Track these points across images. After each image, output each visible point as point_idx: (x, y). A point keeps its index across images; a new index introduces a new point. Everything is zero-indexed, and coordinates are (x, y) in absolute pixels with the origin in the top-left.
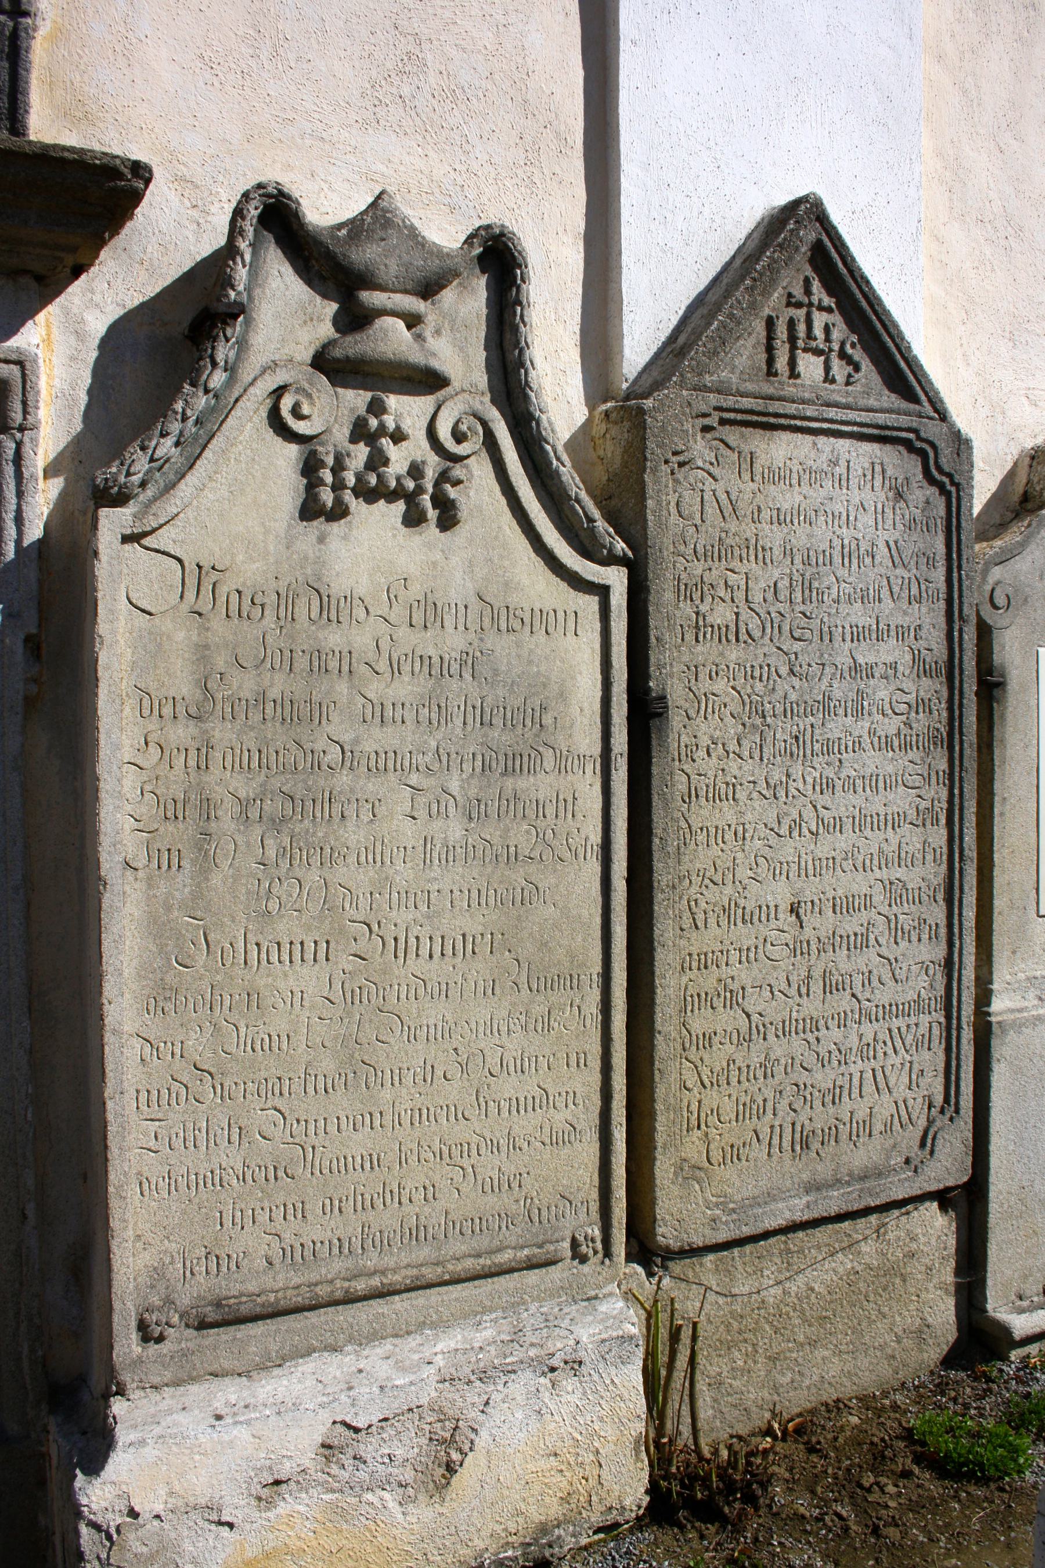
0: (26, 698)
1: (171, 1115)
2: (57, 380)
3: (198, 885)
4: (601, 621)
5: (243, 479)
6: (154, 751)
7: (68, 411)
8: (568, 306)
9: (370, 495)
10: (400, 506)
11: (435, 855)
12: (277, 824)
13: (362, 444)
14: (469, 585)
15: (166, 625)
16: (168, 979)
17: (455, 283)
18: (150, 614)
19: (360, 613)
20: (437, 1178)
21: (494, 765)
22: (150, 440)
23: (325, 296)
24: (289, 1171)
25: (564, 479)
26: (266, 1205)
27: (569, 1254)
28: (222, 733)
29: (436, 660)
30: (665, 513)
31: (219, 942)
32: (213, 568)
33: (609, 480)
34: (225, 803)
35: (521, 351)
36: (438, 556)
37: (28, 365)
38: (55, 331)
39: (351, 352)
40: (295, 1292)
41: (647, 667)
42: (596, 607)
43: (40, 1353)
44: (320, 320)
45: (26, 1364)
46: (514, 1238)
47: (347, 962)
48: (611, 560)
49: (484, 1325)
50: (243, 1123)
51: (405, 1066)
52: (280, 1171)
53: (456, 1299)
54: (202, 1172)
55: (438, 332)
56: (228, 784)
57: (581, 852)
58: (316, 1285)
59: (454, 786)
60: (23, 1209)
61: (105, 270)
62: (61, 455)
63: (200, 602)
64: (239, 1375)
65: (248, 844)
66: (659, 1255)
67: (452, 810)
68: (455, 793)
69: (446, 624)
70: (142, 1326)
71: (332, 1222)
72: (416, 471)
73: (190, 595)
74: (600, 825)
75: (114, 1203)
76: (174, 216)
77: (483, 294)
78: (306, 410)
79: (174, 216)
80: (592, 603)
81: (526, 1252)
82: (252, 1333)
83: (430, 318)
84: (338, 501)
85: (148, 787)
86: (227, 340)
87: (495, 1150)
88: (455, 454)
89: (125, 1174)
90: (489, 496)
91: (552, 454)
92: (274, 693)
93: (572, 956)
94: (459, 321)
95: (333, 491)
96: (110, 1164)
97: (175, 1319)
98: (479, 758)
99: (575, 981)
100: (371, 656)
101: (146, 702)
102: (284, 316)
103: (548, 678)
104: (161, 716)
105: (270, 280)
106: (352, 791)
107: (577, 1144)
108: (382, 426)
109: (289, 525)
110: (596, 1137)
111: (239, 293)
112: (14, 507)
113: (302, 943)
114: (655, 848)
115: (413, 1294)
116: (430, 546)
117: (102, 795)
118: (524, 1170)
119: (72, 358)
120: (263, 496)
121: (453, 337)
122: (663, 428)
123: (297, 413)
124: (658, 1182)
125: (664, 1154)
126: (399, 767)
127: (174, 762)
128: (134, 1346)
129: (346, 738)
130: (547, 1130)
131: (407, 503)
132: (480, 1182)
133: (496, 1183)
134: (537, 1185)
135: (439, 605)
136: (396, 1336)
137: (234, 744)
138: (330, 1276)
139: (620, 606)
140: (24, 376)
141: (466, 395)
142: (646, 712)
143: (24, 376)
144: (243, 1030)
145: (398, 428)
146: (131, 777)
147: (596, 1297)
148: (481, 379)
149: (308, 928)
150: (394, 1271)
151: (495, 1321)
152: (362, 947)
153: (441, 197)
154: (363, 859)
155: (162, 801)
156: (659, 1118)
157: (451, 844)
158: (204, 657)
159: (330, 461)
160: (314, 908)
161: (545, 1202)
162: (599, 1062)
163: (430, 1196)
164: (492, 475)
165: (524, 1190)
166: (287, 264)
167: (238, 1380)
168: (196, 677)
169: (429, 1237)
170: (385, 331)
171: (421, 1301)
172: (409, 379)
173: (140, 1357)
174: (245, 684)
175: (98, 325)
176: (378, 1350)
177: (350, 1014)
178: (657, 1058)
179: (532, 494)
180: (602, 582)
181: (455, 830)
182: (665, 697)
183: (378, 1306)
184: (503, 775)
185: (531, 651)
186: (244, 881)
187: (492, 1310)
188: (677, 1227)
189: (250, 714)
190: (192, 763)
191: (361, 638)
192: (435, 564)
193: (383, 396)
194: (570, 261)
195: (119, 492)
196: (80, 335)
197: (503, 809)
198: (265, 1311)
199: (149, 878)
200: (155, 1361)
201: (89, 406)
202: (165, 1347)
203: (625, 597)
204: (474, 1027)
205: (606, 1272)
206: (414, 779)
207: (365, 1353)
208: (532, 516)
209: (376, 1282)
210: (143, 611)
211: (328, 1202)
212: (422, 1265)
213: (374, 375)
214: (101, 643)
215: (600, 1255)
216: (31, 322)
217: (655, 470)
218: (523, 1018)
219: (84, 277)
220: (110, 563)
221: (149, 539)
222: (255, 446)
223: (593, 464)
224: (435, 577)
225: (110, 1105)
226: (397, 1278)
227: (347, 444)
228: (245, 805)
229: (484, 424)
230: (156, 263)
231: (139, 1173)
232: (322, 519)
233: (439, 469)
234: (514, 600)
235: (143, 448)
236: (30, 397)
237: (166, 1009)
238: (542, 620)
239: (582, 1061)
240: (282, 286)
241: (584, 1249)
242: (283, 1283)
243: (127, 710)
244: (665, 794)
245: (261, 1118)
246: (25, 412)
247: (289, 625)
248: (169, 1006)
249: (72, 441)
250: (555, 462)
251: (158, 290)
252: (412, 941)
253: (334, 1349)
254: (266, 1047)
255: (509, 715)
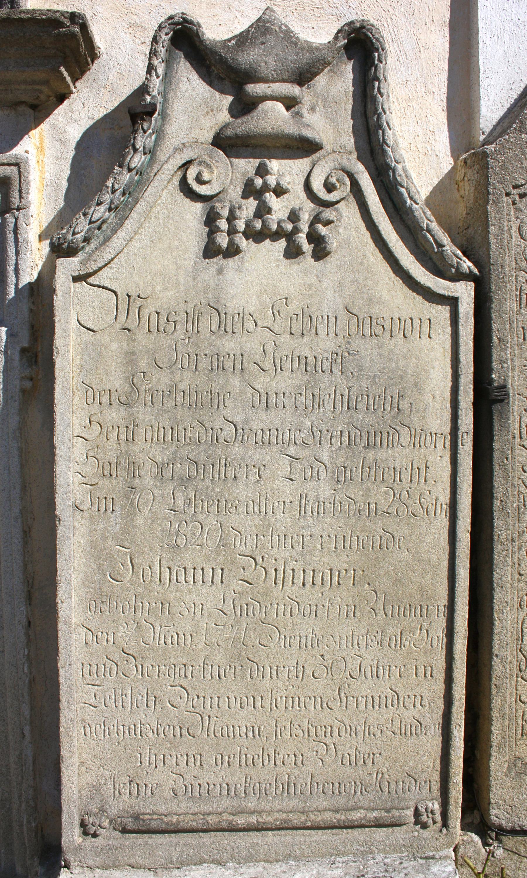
0: (23, 391)
1: (106, 683)
2: (47, 174)
3: (126, 524)
4: (452, 326)
5: (161, 231)
6: (96, 428)
7: (54, 194)
8: (436, 80)
9: (257, 236)
10: (282, 243)
11: (309, 508)
12: (185, 481)
13: (252, 199)
14: (338, 301)
15: (104, 338)
16: (105, 588)
17: (326, 70)
18: (94, 331)
19: (250, 325)
20: (305, 750)
21: (358, 440)
22: (89, 208)
23: (222, 92)
24: (191, 732)
25: (416, 214)
26: (173, 753)
27: (412, 820)
28: (144, 415)
29: (311, 359)
30: (506, 236)
31: (141, 565)
32: (139, 297)
33: (467, 214)
34: (146, 466)
35: (379, 116)
36: (314, 280)
37: (22, 165)
38: (46, 141)
39: (239, 131)
40: (192, 818)
41: (490, 361)
42: (448, 315)
43: (33, 824)
44: (219, 110)
45: (25, 829)
46: (366, 802)
47: (237, 585)
48: (459, 276)
49: (337, 864)
50: (158, 693)
51: (281, 665)
52: (185, 730)
53: (316, 842)
54: (127, 724)
55: (313, 109)
56: (149, 452)
57: (432, 509)
58: (209, 814)
59: (325, 456)
60: (22, 730)
61: (81, 95)
62: (50, 224)
63: (129, 321)
64: (149, 869)
65: (163, 496)
66: (493, 831)
67: (323, 474)
68: (326, 462)
69: (319, 331)
70: (83, 824)
71: (222, 772)
72: (294, 216)
73: (122, 317)
74: (449, 489)
75: (63, 738)
76: (128, 52)
77: (350, 76)
78: (206, 176)
79: (128, 52)
80: (445, 311)
81: (375, 814)
82: (159, 841)
83: (306, 99)
84: (231, 243)
85: (91, 454)
86: (145, 132)
87: (353, 734)
88: (326, 201)
89: (72, 720)
90: (356, 231)
91: (406, 195)
92: (183, 386)
93: (422, 591)
94: (330, 99)
95: (228, 235)
96: (62, 712)
97: (106, 823)
98: (346, 434)
99: (424, 611)
100: (258, 357)
101: (90, 393)
102: (194, 109)
103: (405, 372)
104: (100, 404)
105: (181, 85)
106: (242, 458)
107: (422, 737)
108: (265, 184)
109: (196, 263)
110: (439, 732)
111: (153, 97)
112: (14, 262)
113: (203, 569)
114: (495, 508)
115: (283, 832)
116: (306, 272)
117: (58, 458)
118: (376, 751)
119: (58, 158)
120: (176, 243)
121: (326, 112)
122: (504, 167)
123: (199, 180)
124: (492, 773)
125: (498, 752)
126: (280, 441)
127: (110, 435)
128: (76, 838)
129: (238, 419)
130: (397, 723)
131: (288, 241)
132: (340, 756)
133: (353, 758)
134: (387, 765)
135: (314, 317)
136: (267, 861)
137: (153, 423)
138: (219, 810)
139: (467, 313)
140: (20, 172)
141: (336, 155)
142: (488, 399)
143: (20, 172)
144: (158, 628)
145: (278, 184)
146: (79, 446)
147: (433, 857)
148: (349, 141)
149: (208, 559)
150: (269, 813)
151: (347, 863)
152: (249, 574)
153: (329, 10)
154: (251, 509)
155: (101, 464)
156: (494, 723)
157: (321, 500)
158: (131, 361)
159: (225, 213)
160: (213, 544)
161: (394, 777)
162: (443, 675)
163: (299, 762)
164: (359, 215)
165: (377, 766)
166: (194, 72)
167: (148, 873)
168: (126, 375)
169: (298, 792)
170: (266, 112)
171: (288, 839)
172: (288, 147)
173: (80, 846)
174: (161, 380)
175: (75, 134)
176: (252, 870)
177: (238, 623)
178: (494, 676)
179: (391, 227)
180: (451, 294)
181: (325, 490)
182: (505, 387)
183: (255, 837)
184: (365, 448)
185: (391, 351)
186: (159, 522)
187: (344, 854)
188: (509, 810)
189: (165, 402)
190: (123, 437)
191: (251, 345)
192: (310, 286)
193: (267, 161)
194: (437, 44)
195: (68, 246)
196: (63, 142)
197: (366, 474)
198: (168, 828)
199: (92, 517)
200: (90, 850)
201: (68, 190)
202: (97, 841)
203: (472, 306)
204: (337, 639)
205: (442, 838)
206: (292, 450)
207: (242, 870)
208: (391, 245)
209: (253, 819)
210: (89, 329)
211: (219, 757)
212: (291, 812)
213: (261, 146)
214: (58, 353)
215: (439, 824)
216: (27, 136)
217: (496, 203)
218: (379, 636)
219: (66, 102)
220: (63, 297)
221: (92, 278)
222: (169, 206)
223: (457, 202)
224: (310, 296)
225: (62, 672)
226: (270, 819)
227: (240, 200)
228: (161, 467)
229: (351, 176)
230: (115, 86)
231: (83, 720)
232: (221, 256)
233: (314, 214)
234: (376, 311)
235: (85, 215)
236: (24, 187)
237: (103, 609)
238: (401, 327)
239: (429, 673)
240: (190, 88)
241: (424, 818)
242: (183, 810)
243: (77, 399)
244: (505, 465)
245: (171, 692)
246: (21, 197)
247: (194, 336)
248: (105, 608)
249: (57, 214)
250: (409, 201)
251: (116, 104)
252: (289, 572)
253: (219, 863)
254: (175, 642)
255: (371, 401)
